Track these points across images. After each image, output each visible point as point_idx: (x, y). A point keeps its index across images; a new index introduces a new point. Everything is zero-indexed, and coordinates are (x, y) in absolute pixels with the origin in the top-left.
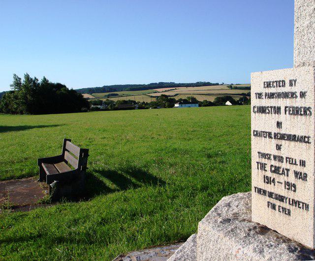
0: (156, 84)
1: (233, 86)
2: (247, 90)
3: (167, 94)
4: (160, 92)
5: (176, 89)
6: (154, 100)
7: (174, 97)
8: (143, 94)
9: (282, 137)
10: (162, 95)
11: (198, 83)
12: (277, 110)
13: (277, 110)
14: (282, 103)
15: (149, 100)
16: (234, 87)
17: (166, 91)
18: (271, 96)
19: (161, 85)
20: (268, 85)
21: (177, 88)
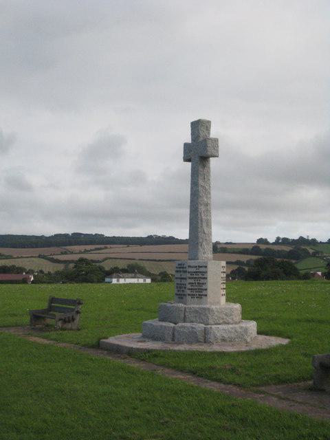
0: (66, 236)
1: (219, 246)
2: (246, 256)
3: (88, 256)
4: (76, 253)
5: (106, 248)
6: (61, 267)
7: (101, 264)
8: (40, 256)
9: (182, 278)
10: (81, 260)
11: (150, 237)
12: (180, 271)
13: (180, 271)
14: (182, 269)
15: (49, 268)
16: (222, 248)
17: (86, 251)
18: (179, 268)
19: (77, 239)
20: (179, 265)
21: (108, 246)
